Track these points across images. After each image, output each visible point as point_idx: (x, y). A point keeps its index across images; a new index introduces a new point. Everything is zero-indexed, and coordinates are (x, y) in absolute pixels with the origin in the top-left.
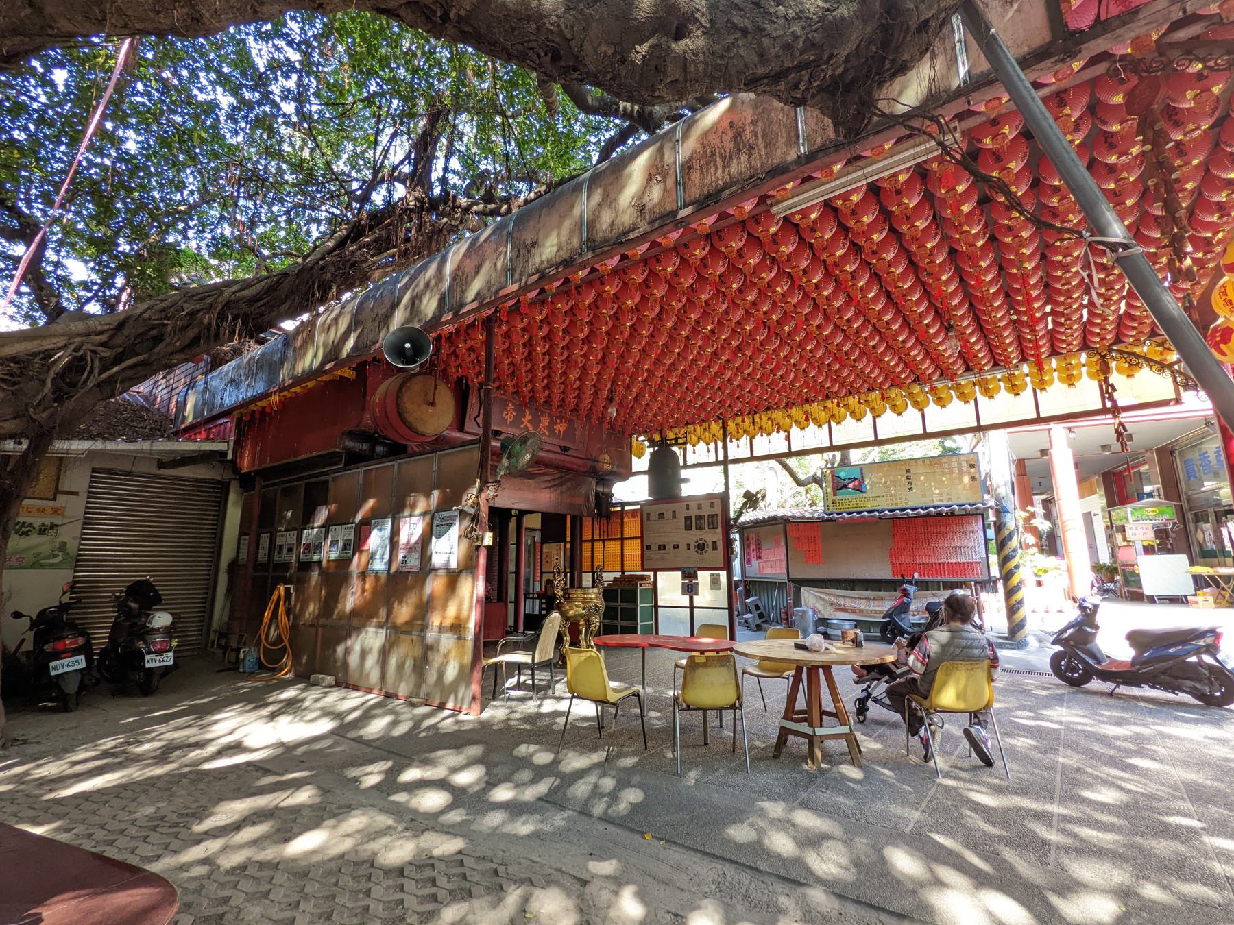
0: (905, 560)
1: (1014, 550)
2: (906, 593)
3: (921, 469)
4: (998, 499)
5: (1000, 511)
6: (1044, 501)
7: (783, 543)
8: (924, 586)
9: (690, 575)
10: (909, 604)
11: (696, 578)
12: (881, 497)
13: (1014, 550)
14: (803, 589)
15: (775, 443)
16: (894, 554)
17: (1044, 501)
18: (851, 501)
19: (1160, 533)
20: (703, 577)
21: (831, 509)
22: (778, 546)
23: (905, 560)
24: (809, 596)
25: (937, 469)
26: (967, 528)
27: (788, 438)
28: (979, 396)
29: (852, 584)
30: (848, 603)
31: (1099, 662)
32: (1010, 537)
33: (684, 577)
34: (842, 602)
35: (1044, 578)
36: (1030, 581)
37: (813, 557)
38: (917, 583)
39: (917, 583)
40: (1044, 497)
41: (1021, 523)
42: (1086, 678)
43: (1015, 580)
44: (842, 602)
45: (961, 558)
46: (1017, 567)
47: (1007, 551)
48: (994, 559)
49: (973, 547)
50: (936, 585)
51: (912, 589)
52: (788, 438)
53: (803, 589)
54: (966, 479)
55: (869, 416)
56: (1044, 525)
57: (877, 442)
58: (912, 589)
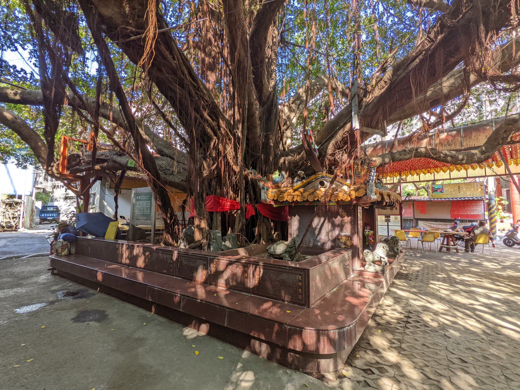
0: (456, 213)
1: (494, 211)
2: (456, 223)
3: (464, 186)
4: (490, 195)
5: (490, 199)
6: (507, 191)
7: (412, 207)
8: (462, 221)
9: (387, 216)
10: (456, 227)
11: (390, 217)
12: (448, 194)
13: (494, 211)
14: (419, 221)
15: (416, 178)
16: (452, 212)
17: (507, 191)
18: (438, 196)
19: (339, 239)
20: (392, 218)
21: (431, 197)
22: (410, 207)
23: (456, 213)
24: (421, 224)
25: (469, 186)
26: (478, 204)
27: (419, 177)
28: (486, 168)
29: (436, 220)
30: (435, 226)
31: (517, 240)
32: (493, 207)
33: (386, 217)
34: (433, 225)
35: (505, 220)
36: (499, 220)
37: (423, 211)
38: (460, 220)
39: (460, 220)
40: (507, 189)
41: (497, 202)
42: (513, 245)
43: (493, 220)
44: (433, 225)
45: (475, 213)
46: (494, 216)
47: (491, 211)
48: (487, 213)
49: (480, 210)
50: (466, 221)
51: (458, 222)
52: (419, 177)
53: (419, 221)
54: (480, 190)
55: (448, 171)
56: (505, 203)
57: (450, 179)
58: (458, 222)
